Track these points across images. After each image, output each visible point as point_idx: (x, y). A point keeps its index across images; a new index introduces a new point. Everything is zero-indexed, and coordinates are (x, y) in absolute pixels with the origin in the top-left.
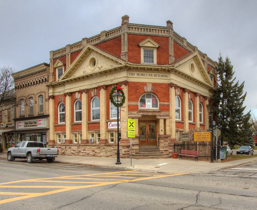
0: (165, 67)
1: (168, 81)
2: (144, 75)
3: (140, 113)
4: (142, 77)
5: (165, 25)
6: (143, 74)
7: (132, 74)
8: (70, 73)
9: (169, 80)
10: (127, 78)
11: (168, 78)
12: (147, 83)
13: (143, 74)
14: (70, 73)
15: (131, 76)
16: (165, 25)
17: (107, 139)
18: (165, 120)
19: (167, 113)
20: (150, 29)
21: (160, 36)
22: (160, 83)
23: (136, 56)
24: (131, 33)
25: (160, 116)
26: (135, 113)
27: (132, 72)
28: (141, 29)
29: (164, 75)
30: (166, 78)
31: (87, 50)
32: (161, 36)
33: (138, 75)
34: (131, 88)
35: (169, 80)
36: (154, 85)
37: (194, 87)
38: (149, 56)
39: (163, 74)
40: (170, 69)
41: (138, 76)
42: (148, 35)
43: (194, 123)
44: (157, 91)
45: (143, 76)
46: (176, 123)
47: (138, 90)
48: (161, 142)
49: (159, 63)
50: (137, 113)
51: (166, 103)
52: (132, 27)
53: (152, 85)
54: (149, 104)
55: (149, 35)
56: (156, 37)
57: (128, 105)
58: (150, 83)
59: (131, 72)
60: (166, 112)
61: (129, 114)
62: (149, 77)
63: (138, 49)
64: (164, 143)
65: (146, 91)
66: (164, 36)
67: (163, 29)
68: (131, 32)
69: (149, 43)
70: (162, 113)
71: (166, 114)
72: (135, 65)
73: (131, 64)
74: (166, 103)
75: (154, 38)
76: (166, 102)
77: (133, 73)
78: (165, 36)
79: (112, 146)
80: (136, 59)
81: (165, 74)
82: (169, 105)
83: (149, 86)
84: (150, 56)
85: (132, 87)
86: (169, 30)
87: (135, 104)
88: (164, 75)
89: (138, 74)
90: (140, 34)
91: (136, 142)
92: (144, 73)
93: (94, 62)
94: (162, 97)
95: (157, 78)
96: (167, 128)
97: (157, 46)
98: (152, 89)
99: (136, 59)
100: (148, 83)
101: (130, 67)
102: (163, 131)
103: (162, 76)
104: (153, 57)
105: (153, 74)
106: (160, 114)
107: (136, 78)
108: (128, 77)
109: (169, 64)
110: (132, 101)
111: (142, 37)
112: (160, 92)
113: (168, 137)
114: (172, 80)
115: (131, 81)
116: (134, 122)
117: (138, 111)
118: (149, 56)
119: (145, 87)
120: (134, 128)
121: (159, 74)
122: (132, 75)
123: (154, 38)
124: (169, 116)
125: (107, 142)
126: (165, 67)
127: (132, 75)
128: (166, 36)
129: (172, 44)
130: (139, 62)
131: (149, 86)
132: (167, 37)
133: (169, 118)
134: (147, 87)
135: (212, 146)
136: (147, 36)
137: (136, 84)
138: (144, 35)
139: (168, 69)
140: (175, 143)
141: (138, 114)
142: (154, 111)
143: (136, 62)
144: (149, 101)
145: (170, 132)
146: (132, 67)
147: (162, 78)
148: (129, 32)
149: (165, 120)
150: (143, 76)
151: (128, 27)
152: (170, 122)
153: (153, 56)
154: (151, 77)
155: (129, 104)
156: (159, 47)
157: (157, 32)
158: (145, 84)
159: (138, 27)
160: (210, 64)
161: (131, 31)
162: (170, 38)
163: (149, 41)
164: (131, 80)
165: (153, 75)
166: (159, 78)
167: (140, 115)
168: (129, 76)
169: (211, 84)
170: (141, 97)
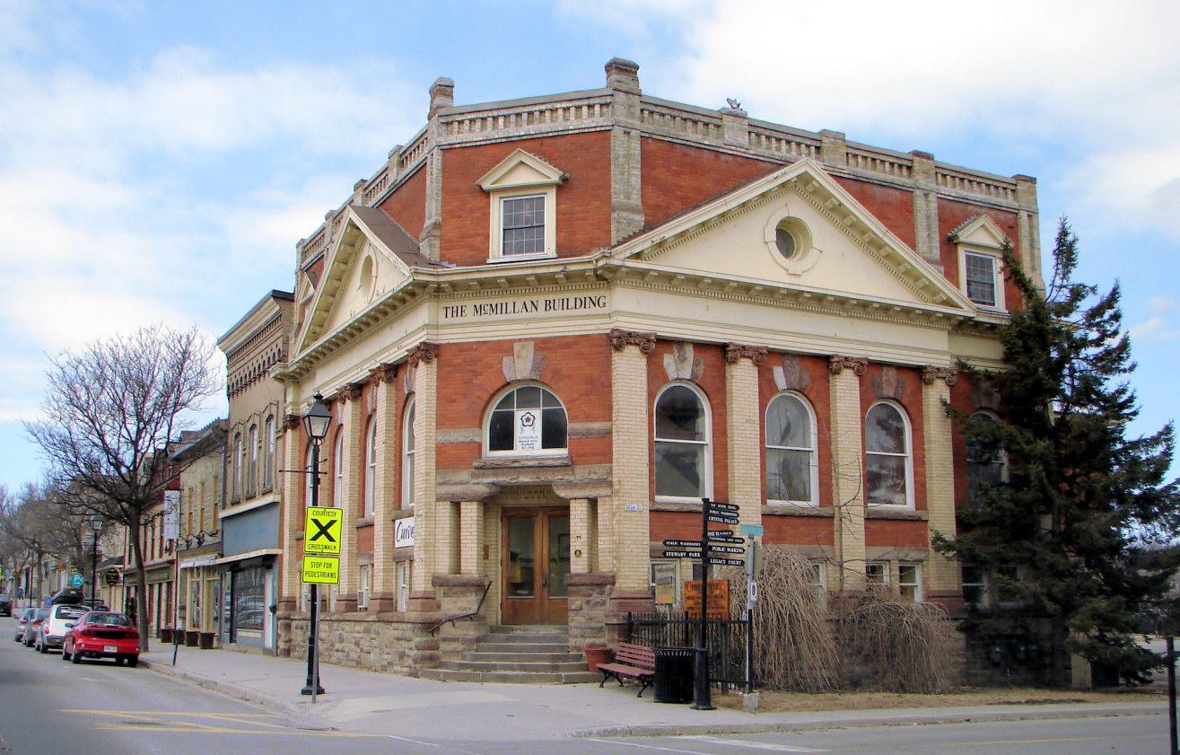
0: (591, 260)
1: (607, 320)
2: (502, 309)
3: (484, 476)
4: (494, 317)
5: (597, 80)
6: (499, 307)
7: (455, 309)
8: (321, 325)
9: (609, 316)
10: (435, 331)
11: (606, 310)
12: (514, 341)
13: (499, 307)
14: (321, 325)
15: (450, 320)
16: (597, 80)
17: (391, 594)
18: (593, 503)
19: (599, 470)
20: (531, 113)
21: (570, 132)
22: (573, 336)
23: (473, 232)
24: (454, 146)
25: (571, 485)
26: (464, 475)
27: (455, 304)
28: (495, 118)
29: (588, 300)
30: (597, 310)
31: (349, 228)
32: (577, 131)
33: (478, 310)
34: (451, 369)
35: (609, 316)
36: (543, 345)
37: (808, 331)
38: (517, 227)
39: (581, 295)
40: (602, 267)
41: (478, 318)
42: (523, 138)
43: (826, 511)
44: (556, 373)
45: (499, 311)
46: (766, 519)
47: (476, 374)
48: (573, 607)
49: (563, 250)
50: (472, 477)
51: (597, 426)
52: (460, 118)
53: (535, 350)
54: (528, 432)
55: (525, 137)
56: (558, 139)
57: (437, 444)
58: (526, 340)
59: (450, 304)
60: (596, 468)
61: (440, 484)
62: (524, 315)
63: (479, 201)
64: (585, 610)
65: (509, 376)
66: (586, 130)
67: (586, 102)
68: (454, 142)
69: (530, 172)
70: (580, 473)
71: (595, 477)
72: (475, 274)
73: (454, 272)
74: (597, 426)
75: (540, 145)
76: (595, 419)
77: (459, 304)
78: (593, 130)
79: (394, 624)
80: (472, 247)
81: (594, 294)
82: (607, 435)
83: (524, 353)
84: (520, 226)
85: (454, 366)
86: (609, 101)
87: (461, 439)
88: (588, 300)
89: (478, 307)
90: (488, 142)
91: (465, 605)
92: (504, 301)
93: (788, 238)
94: (577, 399)
95: (560, 312)
96: (604, 543)
97: (555, 176)
98: (535, 368)
99: (472, 247)
100: (519, 340)
101: (439, 283)
102: (585, 555)
103: (578, 306)
104: (543, 226)
105: (469, 306)
106: (567, 477)
107: (468, 326)
108: (437, 327)
109: (613, 244)
110: (453, 427)
111: (496, 150)
112: (570, 377)
113: (601, 585)
114: (621, 318)
115: (451, 341)
116: (338, 517)
117: (476, 468)
118: (523, 230)
119: (506, 360)
120: (337, 544)
121: (565, 296)
122: (455, 314)
123: (540, 145)
124: (610, 484)
125: (392, 604)
126: (591, 260)
127: (455, 314)
128: (598, 129)
129: (628, 156)
130: (481, 257)
131: (524, 353)
132: (603, 129)
133: (608, 492)
134: (516, 357)
135: (687, 626)
136: (511, 144)
137: (471, 349)
138: (504, 140)
139: (595, 270)
140: (630, 614)
141: (477, 481)
142: (542, 467)
143: (472, 257)
144: (528, 420)
145: (615, 562)
146: (445, 282)
147: (581, 311)
148: (444, 143)
149: (593, 503)
150: (499, 311)
151: (447, 124)
152: (614, 514)
153: (543, 222)
154: (534, 314)
155: (442, 439)
156: (565, 180)
157: (560, 119)
158: (505, 348)
159: (480, 115)
160: (964, 193)
161: (455, 138)
162: (617, 132)
163: (522, 163)
164: (446, 337)
165: (470, 310)
166: (566, 312)
167: (482, 486)
168: (442, 320)
169: (948, 302)
170: (495, 406)
